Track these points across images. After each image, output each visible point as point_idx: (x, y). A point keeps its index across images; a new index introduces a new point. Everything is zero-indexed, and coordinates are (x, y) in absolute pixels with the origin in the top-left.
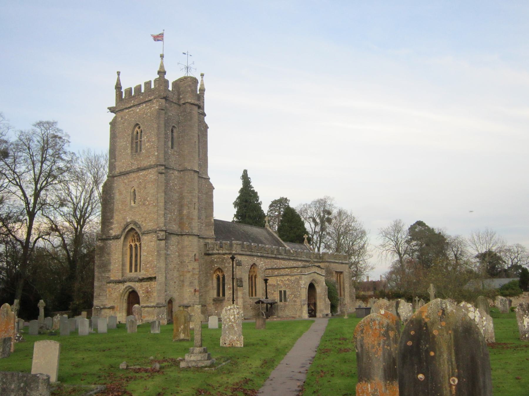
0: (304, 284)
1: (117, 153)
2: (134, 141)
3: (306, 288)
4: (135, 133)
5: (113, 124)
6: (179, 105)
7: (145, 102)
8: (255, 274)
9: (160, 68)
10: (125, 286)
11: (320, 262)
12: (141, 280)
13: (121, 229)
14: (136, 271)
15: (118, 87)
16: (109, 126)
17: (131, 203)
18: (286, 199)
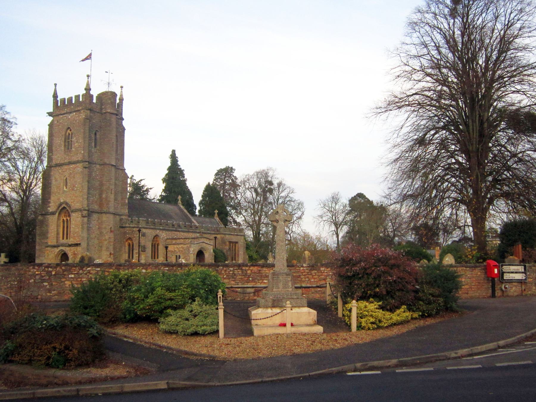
0: (193, 251)
1: (54, 148)
2: (67, 140)
3: (194, 254)
4: (67, 134)
5: (51, 126)
6: (102, 114)
7: (75, 111)
8: (157, 243)
9: (86, 86)
10: (59, 250)
11: (217, 234)
12: (70, 246)
13: (56, 208)
14: (67, 238)
15: (55, 96)
16: (48, 127)
17: (63, 188)
18: (232, 168)
